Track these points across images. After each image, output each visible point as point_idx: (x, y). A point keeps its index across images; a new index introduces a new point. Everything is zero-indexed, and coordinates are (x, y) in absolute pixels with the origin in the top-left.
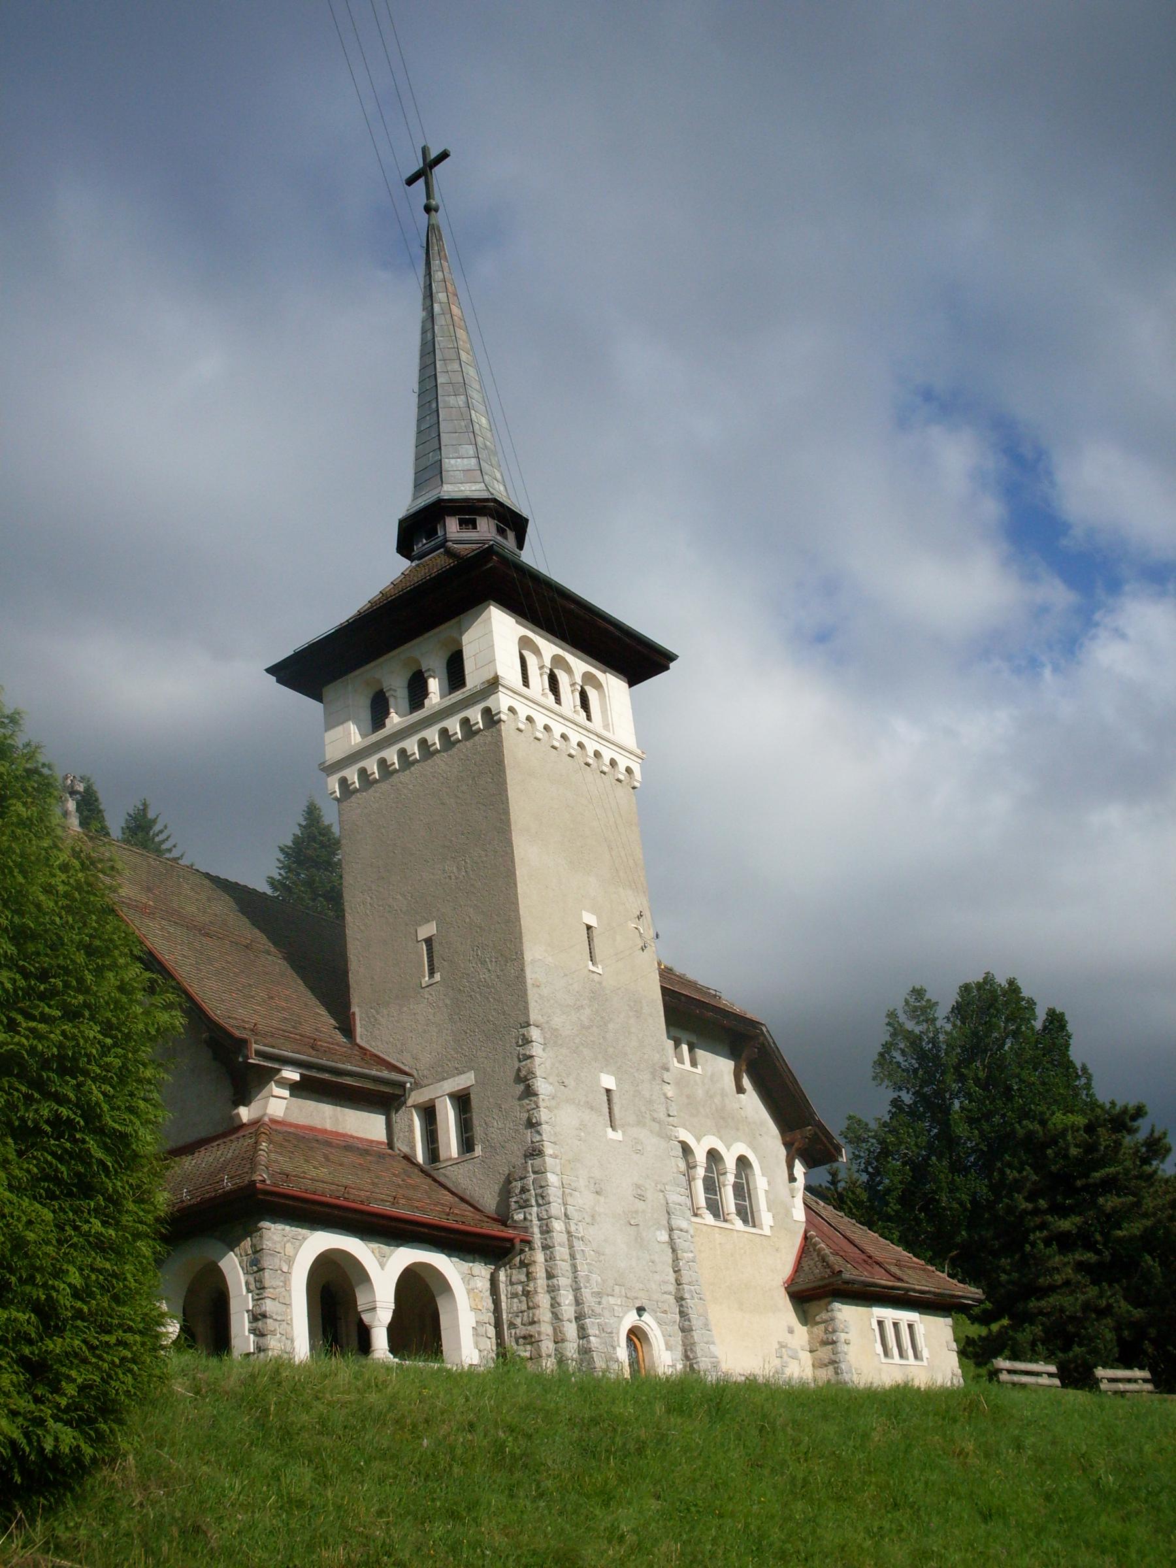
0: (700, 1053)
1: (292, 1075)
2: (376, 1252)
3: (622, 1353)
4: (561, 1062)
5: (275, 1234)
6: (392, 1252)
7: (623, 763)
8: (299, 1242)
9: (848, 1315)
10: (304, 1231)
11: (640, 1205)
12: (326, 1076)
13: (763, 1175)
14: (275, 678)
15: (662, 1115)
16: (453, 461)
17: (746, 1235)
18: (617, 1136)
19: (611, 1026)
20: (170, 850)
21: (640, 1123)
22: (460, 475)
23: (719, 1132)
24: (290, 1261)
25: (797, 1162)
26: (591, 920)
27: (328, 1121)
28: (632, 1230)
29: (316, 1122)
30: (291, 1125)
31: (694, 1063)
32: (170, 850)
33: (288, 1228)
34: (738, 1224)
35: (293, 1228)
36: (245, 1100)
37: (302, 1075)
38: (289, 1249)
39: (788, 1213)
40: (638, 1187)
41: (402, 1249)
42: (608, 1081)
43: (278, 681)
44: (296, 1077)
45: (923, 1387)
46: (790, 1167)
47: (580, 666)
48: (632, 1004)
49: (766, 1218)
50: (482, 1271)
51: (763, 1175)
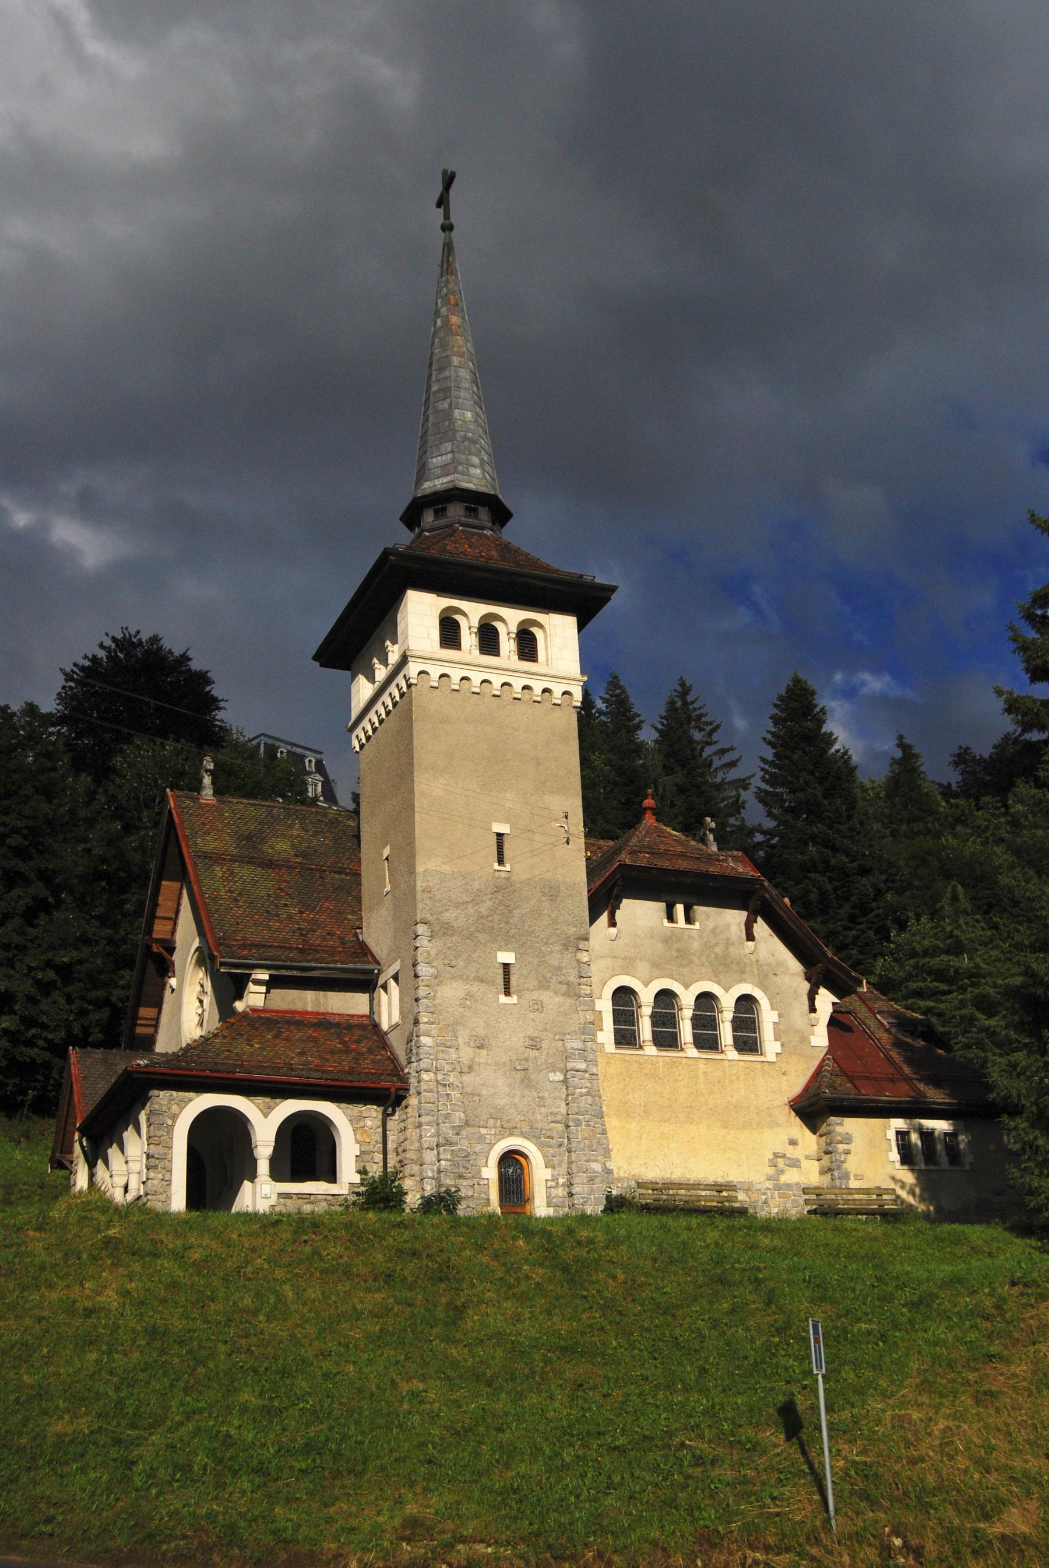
0: (700, 910)
1: (264, 976)
2: (262, 1106)
3: (490, 1172)
4: (449, 948)
5: (162, 1098)
6: (277, 1105)
7: (558, 689)
8: (183, 1104)
9: (851, 1125)
10: (192, 1094)
11: (533, 1053)
12: (295, 973)
13: (773, 1008)
14: (318, 664)
15: (572, 978)
16: (434, 460)
17: (742, 1063)
18: (514, 999)
19: (516, 912)
20: (693, 702)
21: (543, 985)
22: (438, 471)
23: (716, 976)
24: (175, 1118)
25: (822, 991)
26: (504, 828)
27: (310, 1005)
28: (519, 1076)
29: (298, 1007)
30: (272, 1011)
31: (689, 920)
32: (693, 702)
33: (174, 1093)
34: (732, 1054)
35: (180, 1093)
36: (240, 997)
37: (270, 975)
38: (175, 1108)
39: (804, 1039)
40: (532, 1039)
41: (290, 1101)
42: (507, 957)
43: (321, 666)
44: (266, 977)
45: (261, 1211)
46: (812, 996)
47: (512, 617)
48: (547, 890)
49: (771, 1047)
50: (372, 1113)
51: (773, 1008)
